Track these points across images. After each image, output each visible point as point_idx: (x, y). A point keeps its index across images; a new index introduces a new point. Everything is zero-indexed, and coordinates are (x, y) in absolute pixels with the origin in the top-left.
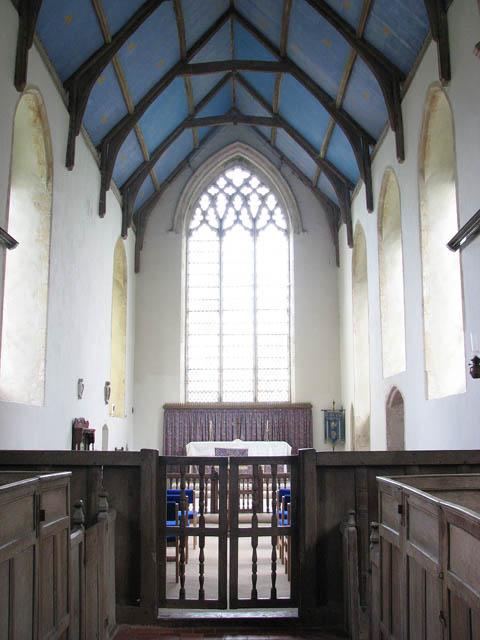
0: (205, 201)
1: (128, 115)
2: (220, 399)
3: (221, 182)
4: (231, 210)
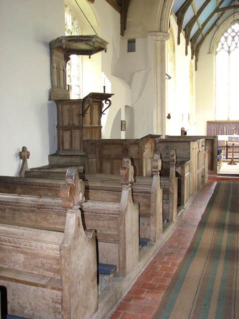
0: (223, 39)
1: (195, 16)
2: (228, 119)
3: (230, 31)
4: (234, 43)
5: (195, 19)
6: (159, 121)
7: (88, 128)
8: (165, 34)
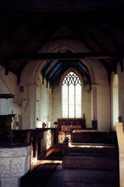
0: (65, 79)
2: (68, 117)
3: (68, 75)
5: (51, 71)
6: (33, 122)
7: (6, 127)
8: (36, 85)
